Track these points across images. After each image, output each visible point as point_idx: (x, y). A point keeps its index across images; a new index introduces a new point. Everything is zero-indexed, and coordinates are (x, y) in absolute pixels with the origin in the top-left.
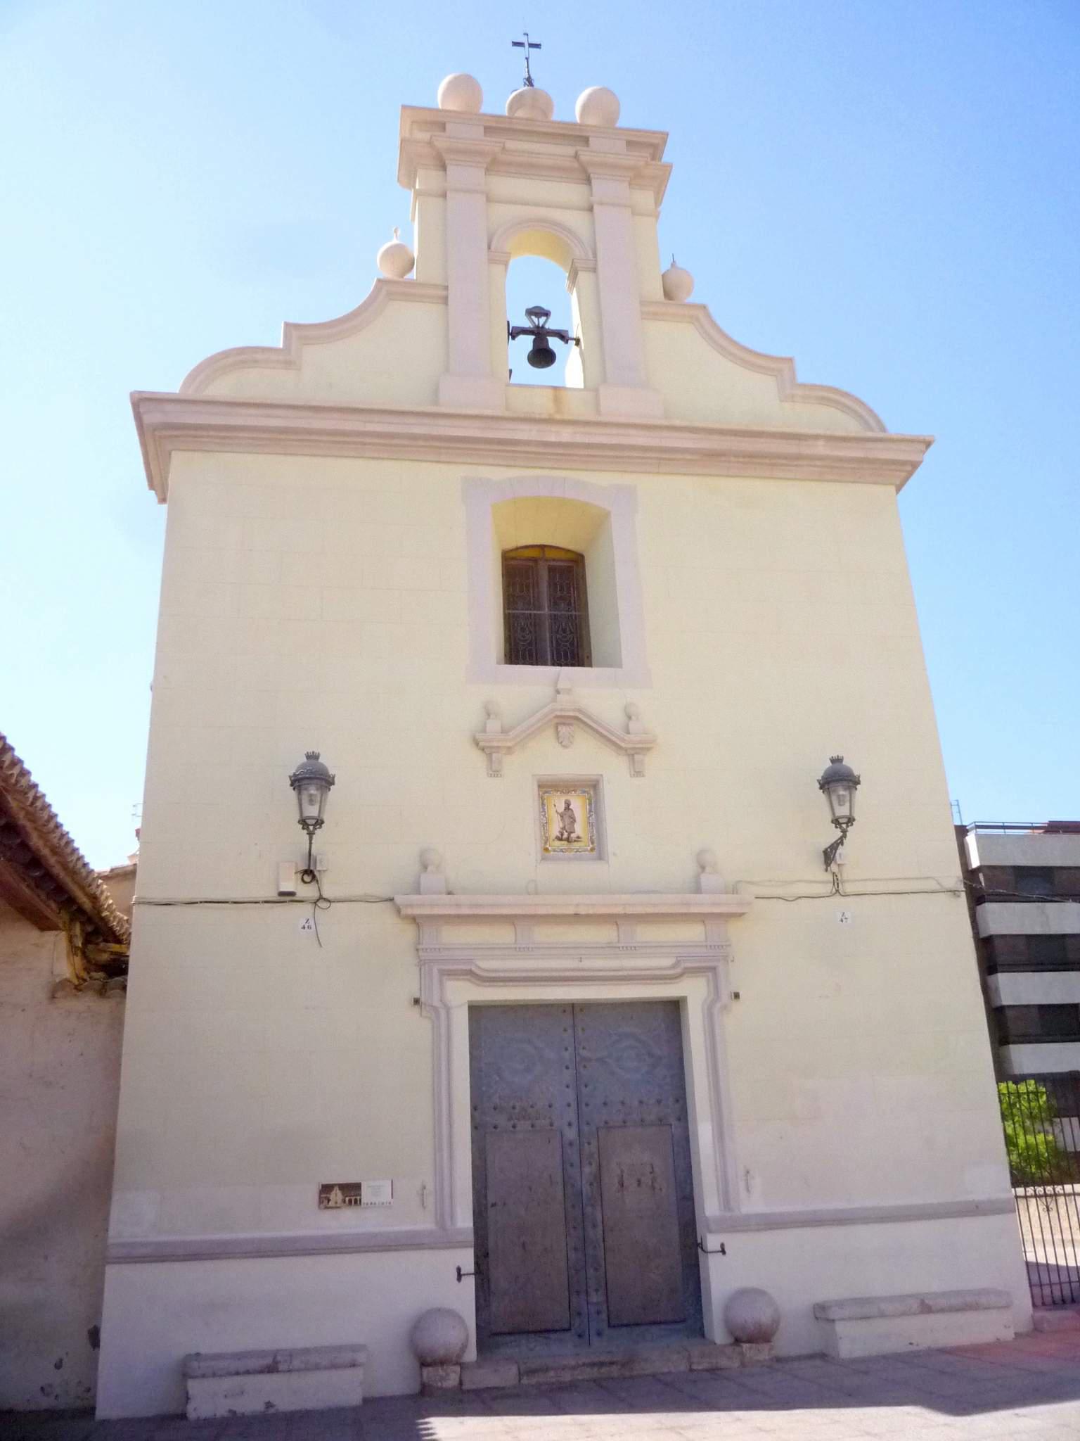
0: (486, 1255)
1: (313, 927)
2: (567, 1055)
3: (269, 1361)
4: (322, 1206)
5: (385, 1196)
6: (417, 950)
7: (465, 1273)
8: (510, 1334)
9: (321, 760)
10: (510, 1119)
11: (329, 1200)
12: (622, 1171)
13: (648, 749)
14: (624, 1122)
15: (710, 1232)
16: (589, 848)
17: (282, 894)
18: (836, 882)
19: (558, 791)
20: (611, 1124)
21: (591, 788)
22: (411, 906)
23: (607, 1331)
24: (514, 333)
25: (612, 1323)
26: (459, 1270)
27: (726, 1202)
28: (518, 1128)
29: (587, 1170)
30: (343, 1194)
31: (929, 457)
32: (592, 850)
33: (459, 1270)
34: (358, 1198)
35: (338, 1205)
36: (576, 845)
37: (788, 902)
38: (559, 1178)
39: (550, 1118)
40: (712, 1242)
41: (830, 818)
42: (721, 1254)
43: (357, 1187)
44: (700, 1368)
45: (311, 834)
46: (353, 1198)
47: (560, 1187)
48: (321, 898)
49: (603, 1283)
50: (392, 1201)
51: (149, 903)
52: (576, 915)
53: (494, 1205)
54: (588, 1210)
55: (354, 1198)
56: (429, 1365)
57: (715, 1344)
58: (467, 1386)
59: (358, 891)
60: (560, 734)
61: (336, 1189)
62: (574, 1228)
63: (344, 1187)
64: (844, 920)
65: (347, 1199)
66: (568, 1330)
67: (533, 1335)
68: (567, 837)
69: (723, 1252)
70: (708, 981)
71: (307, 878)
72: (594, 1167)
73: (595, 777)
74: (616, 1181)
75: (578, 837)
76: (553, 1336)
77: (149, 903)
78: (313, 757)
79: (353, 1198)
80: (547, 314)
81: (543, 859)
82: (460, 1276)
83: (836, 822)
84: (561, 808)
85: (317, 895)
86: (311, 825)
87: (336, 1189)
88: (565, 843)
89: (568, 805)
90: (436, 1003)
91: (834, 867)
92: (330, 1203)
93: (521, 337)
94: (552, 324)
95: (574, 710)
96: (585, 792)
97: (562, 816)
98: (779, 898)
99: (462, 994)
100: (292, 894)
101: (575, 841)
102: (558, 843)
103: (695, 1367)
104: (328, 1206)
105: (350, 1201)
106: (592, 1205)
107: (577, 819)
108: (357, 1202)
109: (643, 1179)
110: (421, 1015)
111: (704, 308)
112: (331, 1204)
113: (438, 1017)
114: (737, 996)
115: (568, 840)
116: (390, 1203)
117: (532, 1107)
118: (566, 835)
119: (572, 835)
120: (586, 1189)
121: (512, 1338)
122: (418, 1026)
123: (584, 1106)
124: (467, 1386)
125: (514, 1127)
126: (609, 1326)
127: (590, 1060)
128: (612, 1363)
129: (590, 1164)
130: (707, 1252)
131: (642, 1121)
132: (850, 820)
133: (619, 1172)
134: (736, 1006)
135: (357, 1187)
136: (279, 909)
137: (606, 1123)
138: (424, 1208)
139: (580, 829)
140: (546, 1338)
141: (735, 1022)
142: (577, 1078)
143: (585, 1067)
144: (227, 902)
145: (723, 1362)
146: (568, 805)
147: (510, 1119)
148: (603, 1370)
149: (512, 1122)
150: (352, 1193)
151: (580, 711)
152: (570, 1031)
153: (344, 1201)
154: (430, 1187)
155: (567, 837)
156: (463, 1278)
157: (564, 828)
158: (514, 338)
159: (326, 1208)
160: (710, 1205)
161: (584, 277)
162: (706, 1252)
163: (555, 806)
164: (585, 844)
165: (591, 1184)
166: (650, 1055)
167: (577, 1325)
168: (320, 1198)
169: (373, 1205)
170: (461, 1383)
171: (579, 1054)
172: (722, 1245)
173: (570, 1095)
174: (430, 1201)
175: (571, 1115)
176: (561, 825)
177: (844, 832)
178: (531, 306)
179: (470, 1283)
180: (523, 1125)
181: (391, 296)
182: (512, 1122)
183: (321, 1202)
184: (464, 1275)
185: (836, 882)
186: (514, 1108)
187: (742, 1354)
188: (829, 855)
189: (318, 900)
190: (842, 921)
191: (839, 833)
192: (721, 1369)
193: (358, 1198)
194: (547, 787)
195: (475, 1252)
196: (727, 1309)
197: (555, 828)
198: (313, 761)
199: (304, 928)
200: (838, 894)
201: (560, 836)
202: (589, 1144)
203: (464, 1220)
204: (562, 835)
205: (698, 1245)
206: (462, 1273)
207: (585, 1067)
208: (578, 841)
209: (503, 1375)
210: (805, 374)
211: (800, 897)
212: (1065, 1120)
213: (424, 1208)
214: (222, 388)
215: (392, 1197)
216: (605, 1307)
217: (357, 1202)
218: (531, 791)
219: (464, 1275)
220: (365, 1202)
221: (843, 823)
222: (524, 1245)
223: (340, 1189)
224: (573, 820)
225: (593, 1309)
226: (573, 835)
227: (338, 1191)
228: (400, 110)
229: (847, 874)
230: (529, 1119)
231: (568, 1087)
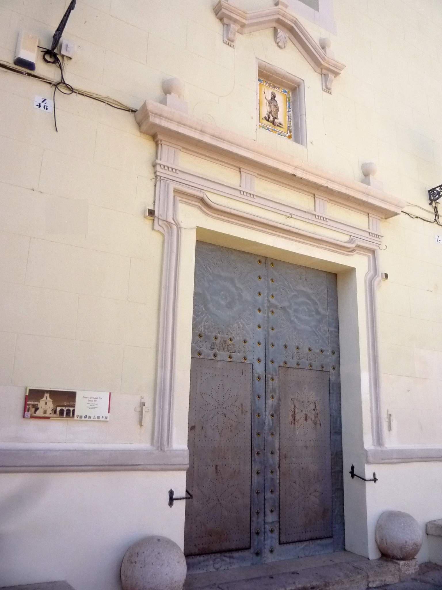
1: (51, 109)
2: (260, 299)
4: (28, 414)
5: (102, 410)
6: (154, 166)
7: (182, 500)
8: (200, 555)
10: (212, 349)
11: (36, 409)
12: (295, 406)
14: (298, 364)
15: (368, 462)
16: (287, 135)
19: (267, 83)
20: (288, 365)
22: (160, 116)
23: (278, 548)
25: (283, 539)
26: (171, 493)
27: (379, 440)
28: (218, 358)
29: (270, 402)
30: (54, 402)
33: (171, 493)
34: (71, 409)
35: (47, 415)
37: (412, 218)
38: (249, 409)
39: (244, 352)
42: (373, 481)
43: (71, 396)
44: (374, 586)
45: (54, 85)
46: (65, 409)
47: (249, 415)
48: (62, 82)
49: (277, 504)
50: (108, 415)
52: (294, 175)
54: (269, 438)
55: (67, 408)
57: (369, 559)
59: (102, 92)
60: (279, 35)
61: (47, 395)
62: (258, 454)
63: (55, 395)
64: (439, 241)
65: (58, 409)
66: (249, 548)
67: (218, 555)
69: (375, 480)
70: (369, 260)
72: (276, 400)
73: (299, 80)
74: (291, 413)
75: (280, 124)
76: (236, 555)
79: (65, 409)
82: (172, 500)
84: (269, 97)
85: (58, 79)
87: (47, 395)
88: (271, 124)
89: (274, 97)
90: (170, 220)
92: (38, 412)
95: (292, 21)
96: (286, 92)
97: (269, 103)
98: (407, 214)
100: (30, 66)
101: (278, 126)
103: (370, 585)
104: (34, 415)
105: (62, 412)
107: (280, 109)
108: (70, 414)
109: (309, 415)
110: (153, 229)
112: (39, 413)
113: (171, 234)
114: (386, 276)
115: (273, 122)
116: (106, 418)
117: (231, 340)
119: (276, 120)
120: (268, 419)
121: (201, 558)
123: (270, 346)
125: (215, 355)
126: (280, 543)
127: (276, 307)
129: (273, 397)
130: (365, 480)
131: (311, 366)
133: (293, 407)
134: (385, 284)
135: (71, 396)
138: (141, 425)
139: (281, 118)
140: (230, 557)
142: (267, 319)
143: (272, 312)
146: (274, 97)
147: (212, 349)
149: (213, 352)
150: (65, 403)
151: (295, 23)
152: (263, 280)
153: (55, 412)
156: (175, 502)
157: (270, 113)
159: (32, 417)
163: (265, 93)
165: (272, 416)
166: (318, 313)
167: (256, 543)
168: (26, 404)
169: (87, 419)
171: (269, 301)
173: (260, 334)
174: (147, 418)
175: (260, 352)
176: (269, 110)
180: (223, 355)
182: (213, 352)
183: (26, 409)
184: (177, 499)
186: (216, 338)
187: (399, 570)
189: (59, 84)
190: (438, 241)
192: (388, 585)
193: (71, 409)
196: (379, 527)
199: (40, 106)
200: (436, 222)
201: (268, 118)
202: (273, 379)
204: (269, 117)
206: (175, 496)
207: (272, 312)
208: (279, 126)
211: (417, 217)
213: (141, 425)
215: (109, 412)
216: (277, 525)
217: (70, 414)
219: (177, 499)
220: (80, 414)
223: (50, 397)
225: (268, 527)
227: (49, 399)
230: (228, 350)
231: (259, 327)
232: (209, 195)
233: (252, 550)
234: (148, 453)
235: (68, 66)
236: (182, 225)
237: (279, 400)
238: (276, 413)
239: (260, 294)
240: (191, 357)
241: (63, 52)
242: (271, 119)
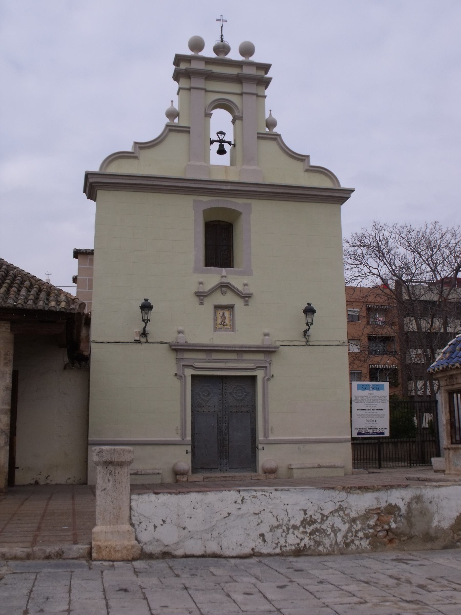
0: (194, 447)
3: (135, 471)
9: (149, 301)
13: (250, 297)
17: (135, 340)
18: (307, 341)
21: (231, 308)
24: (212, 142)
26: (187, 451)
29: (224, 424)
31: (352, 195)
32: (231, 328)
33: (187, 451)
36: (226, 326)
40: (260, 446)
41: (305, 322)
45: (146, 324)
51: (96, 342)
53: (197, 434)
56: (178, 475)
58: (189, 480)
68: (223, 324)
69: (263, 449)
71: (143, 336)
72: (227, 425)
76: (213, 470)
77: (96, 342)
78: (146, 300)
80: (224, 134)
81: (215, 331)
82: (187, 453)
83: (307, 324)
84: (221, 314)
86: (146, 321)
89: (224, 313)
91: (306, 337)
93: (215, 143)
94: (226, 139)
99: (189, 372)
102: (220, 326)
106: (226, 435)
111: (279, 135)
115: (223, 325)
118: (222, 323)
121: (201, 470)
122: (177, 383)
124: (189, 480)
128: (230, 477)
132: (312, 324)
136: (134, 345)
137: (231, 412)
139: (227, 321)
141: (271, 385)
144: (119, 342)
145: (261, 478)
146: (224, 313)
148: (227, 478)
154: (179, 428)
155: (223, 324)
157: (222, 321)
158: (212, 144)
160: (260, 437)
161: (237, 122)
162: (258, 449)
164: (228, 326)
165: (226, 429)
170: (187, 480)
172: (263, 447)
177: (309, 327)
178: (218, 131)
179: (190, 455)
181: (171, 130)
185: (307, 341)
187: (266, 476)
188: (305, 333)
191: (307, 327)
194: (217, 307)
195: (192, 447)
197: (219, 321)
198: (146, 302)
202: (226, 418)
203: (189, 438)
205: (256, 447)
209: (199, 477)
210: (314, 162)
212: (427, 414)
214: (113, 169)
218: (212, 309)
221: (309, 325)
222: (205, 445)
224: (225, 318)
226: (225, 323)
228: (218, 332)
229: (311, 339)
232: (195, 363)
233: (219, 469)
234: (179, 441)
235: (149, 336)
236: (186, 375)
237: (228, 424)
238: (228, 427)
239: (220, 389)
240: (347, 301)
241: (146, 333)
242: (222, 323)
